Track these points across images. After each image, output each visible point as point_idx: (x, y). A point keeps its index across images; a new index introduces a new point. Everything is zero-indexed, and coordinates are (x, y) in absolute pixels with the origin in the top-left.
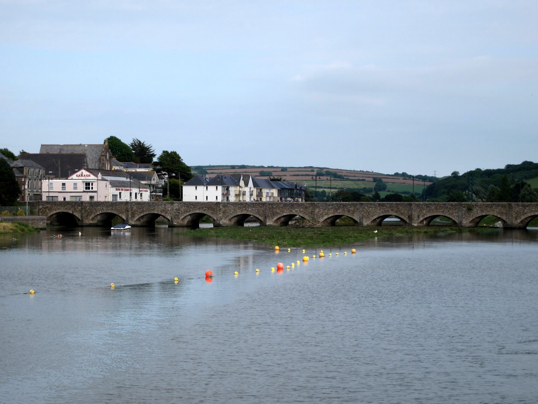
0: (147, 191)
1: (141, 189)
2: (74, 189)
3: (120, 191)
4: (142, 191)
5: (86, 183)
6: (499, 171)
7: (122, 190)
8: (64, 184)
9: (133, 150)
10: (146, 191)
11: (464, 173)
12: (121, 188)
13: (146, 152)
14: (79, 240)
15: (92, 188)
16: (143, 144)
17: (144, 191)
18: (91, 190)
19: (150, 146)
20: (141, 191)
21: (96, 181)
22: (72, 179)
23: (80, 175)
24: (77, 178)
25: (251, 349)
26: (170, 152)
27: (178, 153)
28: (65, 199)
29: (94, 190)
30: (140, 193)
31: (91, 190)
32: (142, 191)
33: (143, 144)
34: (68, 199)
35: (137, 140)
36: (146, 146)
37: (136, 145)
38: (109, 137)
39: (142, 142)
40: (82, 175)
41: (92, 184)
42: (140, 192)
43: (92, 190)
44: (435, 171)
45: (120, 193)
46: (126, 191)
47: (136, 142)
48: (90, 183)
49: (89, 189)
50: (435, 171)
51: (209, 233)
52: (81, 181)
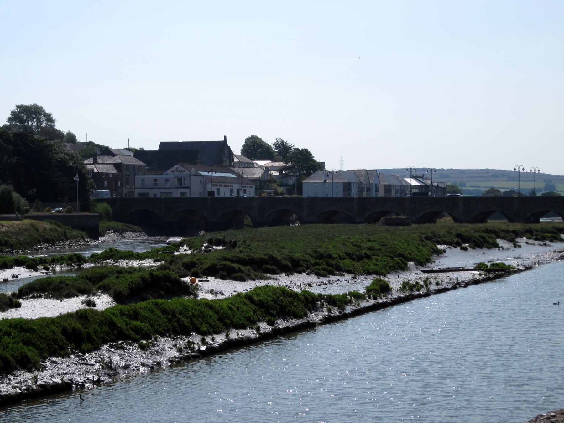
0: (252, 187)
1: (243, 185)
2: (142, 186)
3: (218, 187)
4: (245, 187)
5: (178, 179)
6: (231, 279)
7: (220, 186)
8: (155, 180)
9: (275, 149)
10: (250, 187)
11: (441, 168)
12: (218, 184)
13: (288, 150)
14: (163, 247)
15: (185, 184)
16: (286, 143)
17: (248, 187)
18: (183, 186)
19: (293, 145)
20: (244, 187)
21: (189, 176)
22: (167, 174)
23: (174, 171)
24: (172, 173)
25: (347, 396)
26: (301, 149)
27: (309, 150)
28: (155, 195)
29: (186, 186)
30: (242, 190)
31: (183, 186)
32: (245, 187)
33: (286, 143)
34: (158, 196)
35: (280, 139)
36: (289, 145)
37: (278, 144)
38: (250, 136)
39: (285, 141)
40: (177, 171)
41: (184, 179)
42: (243, 189)
43: (184, 186)
44: (342, 157)
45: (218, 189)
46: (225, 186)
47: (279, 141)
48: (182, 179)
49: (182, 185)
50: (342, 157)
51: (100, 291)
52: (173, 176)
